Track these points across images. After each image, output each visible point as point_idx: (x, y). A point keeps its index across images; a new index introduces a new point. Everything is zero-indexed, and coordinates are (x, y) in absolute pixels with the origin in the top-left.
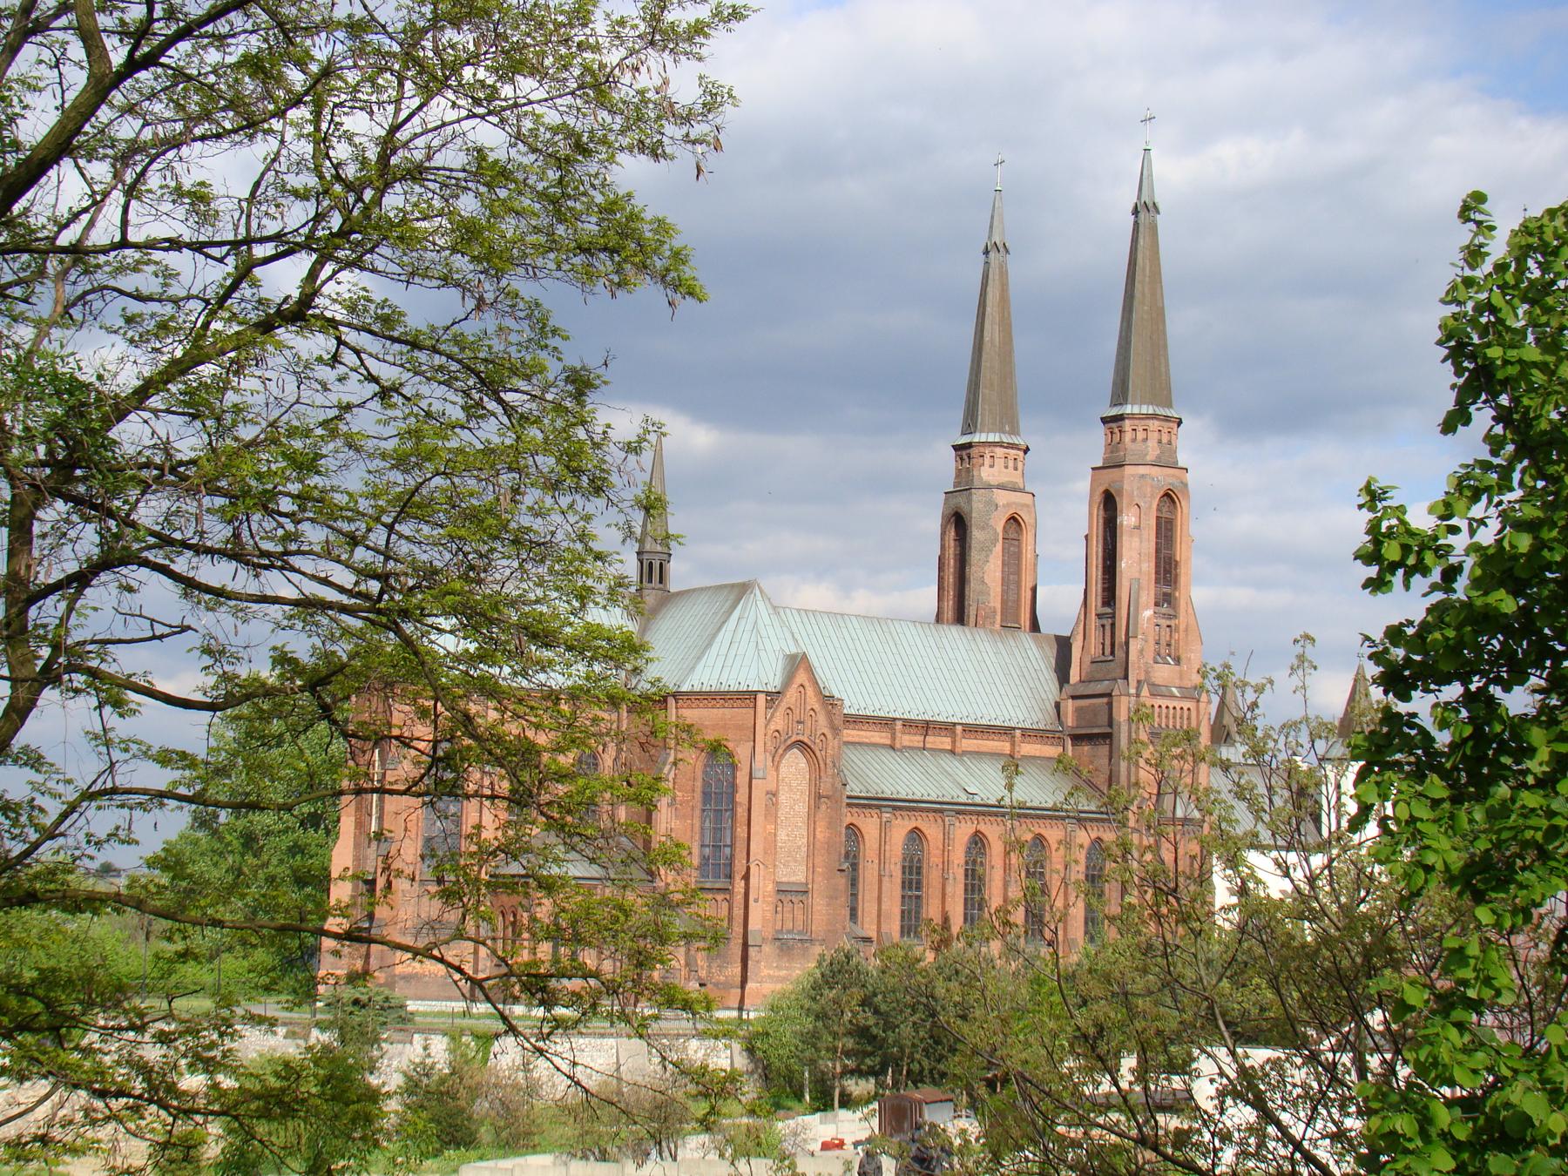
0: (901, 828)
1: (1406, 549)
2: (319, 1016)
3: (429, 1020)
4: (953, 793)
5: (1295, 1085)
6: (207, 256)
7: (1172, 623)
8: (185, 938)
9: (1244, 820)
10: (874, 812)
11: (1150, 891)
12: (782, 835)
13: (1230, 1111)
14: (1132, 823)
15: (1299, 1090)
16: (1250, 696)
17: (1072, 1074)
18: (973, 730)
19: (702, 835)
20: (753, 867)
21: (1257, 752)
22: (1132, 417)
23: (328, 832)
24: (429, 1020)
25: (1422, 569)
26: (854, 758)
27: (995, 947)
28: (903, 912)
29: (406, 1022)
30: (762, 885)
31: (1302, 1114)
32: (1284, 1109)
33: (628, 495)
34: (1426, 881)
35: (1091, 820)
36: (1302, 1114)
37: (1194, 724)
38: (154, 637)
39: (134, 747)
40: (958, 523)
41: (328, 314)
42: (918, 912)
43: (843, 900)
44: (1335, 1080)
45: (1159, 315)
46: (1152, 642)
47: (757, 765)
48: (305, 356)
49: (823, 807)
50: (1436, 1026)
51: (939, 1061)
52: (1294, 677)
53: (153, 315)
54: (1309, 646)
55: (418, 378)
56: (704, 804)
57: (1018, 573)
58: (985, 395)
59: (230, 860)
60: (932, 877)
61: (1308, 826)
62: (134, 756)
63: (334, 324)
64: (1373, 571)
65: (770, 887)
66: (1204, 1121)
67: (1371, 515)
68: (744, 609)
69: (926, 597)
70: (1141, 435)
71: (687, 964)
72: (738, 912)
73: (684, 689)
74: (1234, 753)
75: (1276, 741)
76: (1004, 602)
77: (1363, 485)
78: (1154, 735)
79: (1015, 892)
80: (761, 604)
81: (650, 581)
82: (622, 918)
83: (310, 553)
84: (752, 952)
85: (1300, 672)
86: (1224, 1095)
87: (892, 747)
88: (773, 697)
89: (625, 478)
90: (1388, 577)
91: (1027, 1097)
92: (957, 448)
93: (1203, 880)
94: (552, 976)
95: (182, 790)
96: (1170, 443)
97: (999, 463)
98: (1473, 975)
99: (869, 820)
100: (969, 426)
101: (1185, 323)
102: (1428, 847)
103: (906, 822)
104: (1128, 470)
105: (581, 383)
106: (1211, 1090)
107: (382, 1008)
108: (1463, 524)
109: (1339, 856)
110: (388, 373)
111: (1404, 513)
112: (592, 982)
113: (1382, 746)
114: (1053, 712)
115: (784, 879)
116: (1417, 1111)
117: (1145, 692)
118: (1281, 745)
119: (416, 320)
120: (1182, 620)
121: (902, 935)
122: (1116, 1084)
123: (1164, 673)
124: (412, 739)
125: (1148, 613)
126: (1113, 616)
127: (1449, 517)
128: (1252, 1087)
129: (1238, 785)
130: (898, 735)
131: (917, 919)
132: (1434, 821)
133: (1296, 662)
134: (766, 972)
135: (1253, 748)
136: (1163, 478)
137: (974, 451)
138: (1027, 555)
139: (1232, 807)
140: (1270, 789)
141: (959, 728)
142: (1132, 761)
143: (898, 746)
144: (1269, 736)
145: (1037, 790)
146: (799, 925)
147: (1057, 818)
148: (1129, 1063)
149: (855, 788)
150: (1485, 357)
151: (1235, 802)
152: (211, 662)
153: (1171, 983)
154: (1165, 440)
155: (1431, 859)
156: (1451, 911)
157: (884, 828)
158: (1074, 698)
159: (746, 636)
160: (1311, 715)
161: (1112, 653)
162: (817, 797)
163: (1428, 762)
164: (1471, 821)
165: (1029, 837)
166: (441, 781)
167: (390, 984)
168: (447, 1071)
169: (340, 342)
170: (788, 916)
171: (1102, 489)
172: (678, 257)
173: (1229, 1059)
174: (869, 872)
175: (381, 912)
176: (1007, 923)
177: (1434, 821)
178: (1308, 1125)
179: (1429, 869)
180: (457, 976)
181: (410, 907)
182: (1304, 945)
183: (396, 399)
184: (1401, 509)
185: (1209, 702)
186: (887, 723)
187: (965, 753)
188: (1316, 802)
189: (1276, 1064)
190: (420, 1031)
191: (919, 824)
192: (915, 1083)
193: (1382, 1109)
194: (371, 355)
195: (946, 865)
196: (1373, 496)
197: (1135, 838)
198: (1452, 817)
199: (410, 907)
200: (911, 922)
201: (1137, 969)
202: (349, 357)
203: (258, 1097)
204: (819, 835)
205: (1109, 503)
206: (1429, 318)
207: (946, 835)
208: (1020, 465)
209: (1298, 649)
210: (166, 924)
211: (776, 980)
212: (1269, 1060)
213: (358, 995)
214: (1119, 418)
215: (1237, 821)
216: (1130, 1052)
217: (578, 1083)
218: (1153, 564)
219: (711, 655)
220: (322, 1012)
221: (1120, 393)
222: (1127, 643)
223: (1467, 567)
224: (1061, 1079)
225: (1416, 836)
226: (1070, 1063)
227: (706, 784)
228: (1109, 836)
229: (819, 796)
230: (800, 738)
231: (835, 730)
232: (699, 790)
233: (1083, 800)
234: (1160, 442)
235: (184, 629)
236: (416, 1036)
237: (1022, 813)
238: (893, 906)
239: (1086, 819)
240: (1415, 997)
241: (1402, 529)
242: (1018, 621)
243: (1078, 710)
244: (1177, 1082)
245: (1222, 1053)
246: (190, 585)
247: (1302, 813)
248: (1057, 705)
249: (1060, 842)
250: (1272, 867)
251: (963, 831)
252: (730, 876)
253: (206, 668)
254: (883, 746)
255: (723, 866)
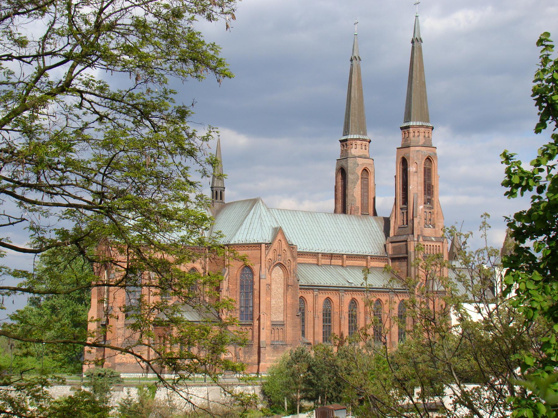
0: (322, 297)
1: (521, 178)
2: (84, 381)
3: (129, 381)
4: (342, 283)
5: (484, 398)
6: (24, 61)
7: (431, 211)
8: (26, 348)
9: (461, 290)
10: (311, 291)
11: (423, 320)
12: (273, 302)
13: (459, 409)
14: (416, 293)
15: (486, 400)
16: (463, 239)
17: (393, 396)
18: (351, 257)
19: (240, 303)
20: (261, 315)
21: (466, 262)
22: (413, 127)
23: (86, 305)
24: (129, 381)
25: (527, 187)
26: (302, 269)
27: (362, 344)
28: (323, 332)
29: (120, 383)
30: (265, 322)
31: (488, 410)
32: (481, 408)
33: (204, 159)
34: (534, 314)
35: (400, 292)
36: (488, 410)
37: (441, 252)
38: (10, 224)
39: (4, 270)
40: (342, 172)
41: (77, 87)
42: (330, 332)
43: (299, 327)
44: (502, 396)
45: (423, 85)
46: (423, 219)
47: (263, 273)
48: (69, 105)
49: (290, 290)
50: (539, 372)
51: (340, 393)
52: (481, 231)
53: (4, 91)
54: (487, 218)
55: (114, 112)
56: (241, 289)
57: (368, 192)
58: (352, 119)
59: (46, 317)
60: (335, 318)
61: (488, 293)
62: (4, 274)
63: (81, 92)
64: (509, 189)
65: (269, 323)
66: (448, 414)
67: (507, 166)
68: (255, 209)
69: (331, 204)
70: (417, 134)
71: (236, 356)
72: (256, 334)
73: (232, 243)
74: (457, 264)
75: (474, 257)
76: (362, 204)
77: (502, 152)
78: (425, 257)
79: (369, 322)
80: (262, 207)
81: (217, 199)
82: (206, 334)
83: (72, 184)
84: (262, 350)
85: (484, 229)
86: (456, 403)
87: (318, 265)
88: (268, 245)
89: (203, 152)
90: (515, 191)
91: (375, 406)
92: (341, 141)
93: (445, 314)
94: (178, 358)
95: (24, 287)
96: (429, 137)
97: (359, 147)
98: (554, 351)
99: (309, 295)
100: (346, 132)
101: (436, 90)
102: (534, 300)
103: (324, 295)
104: (412, 149)
105: (183, 114)
106: (451, 401)
107: (110, 377)
108: (545, 168)
109: (500, 304)
110: (102, 110)
111: (520, 164)
112: (195, 360)
113: (515, 260)
114: (383, 249)
115: (275, 320)
116: (532, 408)
117: (421, 239)
118: (476, 259)
119: (113, 89)
120: (435, 210)
121: (324, 341)
122: (412, 399)
123: (428, 232)
124: (117, 262)
125: (421, 207)
126: (407, 209)
127: (539, 165)
128: (467, 399)
129: (459, 276)
130: (320, 259)
131: (330, 334)
132: (536, 290)
133: (482, 225)
134: (268, 358)
135: (464, 261)
136: (426, 151)
137: (348, 143)
138: (371, 184)
139: (456, 285)
140: (472, 277)
141: (345, 256)
142: (416, 268)
143: (320, 264)
144: (471, 256)
145: (377, 280)
146: (281, 339)
147: (386, 292)
148: (418, 390)
149: (303, 282)
150: (552, 100)
151: (458, 283)
152: (34, 233)
153: (434, 359)
154: (427, 136)
155: (535, 305)
156: (548, 325)
157: (315, 298)
158: (391, 242)
159: (256, 220)
160: (489, 246)
161: (407, 224)
162: (287, 286)
163: (533, 266)
164: (552, 289)
165: (374, 300)
166: (129, 279)
167: (114, 367)
168: (137, 402)
169: (83, 99)
170: (276, 335)
171: (401, 157)
172: (220, 62)
173: (457, 388)
174: (309, 316)
175: (109, 336)
176: (366, 335)
177: (536, 290)
178: (490, 414)
179: (534, 309)
180: (139, 359)
181: (119, 331)
182: (487, 341)
183: (106, 120)
184: (519, 163)
185: (448, 243)
186: (315, 255)
187: (347, 266)
188: (491, 282)
189: (477, 390)
190: (126, 386)
191: (329, 296)
192: (330, 402)
193: (518, 407)
194: (95, 103)
195: (341, 312)
196: (507, 158)
197: (418, 299)
198: (544, 288)
199: (119, 331)
200: (327, 335)
201: (419, 352)
202: (86, 104)
203: (59, 411)
204: (289, 302)
205: (404, 162)
206: (529, 84)
207: (341, 301)
208: (367, 147)
209: (483, 219)
210: (19, 342)
211: (271, 361)
212: (474, 388)
213: (100, 372)
214: (408, 127)
215: (458, 290)
216: (417, 386)
217: (190, 402)
218: (423, 187)
219: (246, 229)
220: (86, 379)
221: (408, 117)
222: (413, 220)
223: (547, 186)
224: (389, 398)
225: (529, 296)
226: (392, 391)
227: (241, 282)
228: (407, 298)
229: (288, 286)
230: (280, 262)
231: (294, 258)
232: (239, 284)
233: (395, 283)
234: (425, 137)
235: (23, 220)
236: (125, 388)
237: (372, 290)
238: (320, 330)
239: (397, 292)
240: (530, 361)
241: (520, 171)
242: (368, 212)
243: (393, 248)
244: (437, 399)
245: (455, 386)
246: (22, 199)
247: (485, 287)
248: (385, 246)
249: (386, 301)
250: (473, 309)
251: (347, 298)
252: (252, 319)
253: (32, 235)
254: (314, 264)
255: (249, 315)
